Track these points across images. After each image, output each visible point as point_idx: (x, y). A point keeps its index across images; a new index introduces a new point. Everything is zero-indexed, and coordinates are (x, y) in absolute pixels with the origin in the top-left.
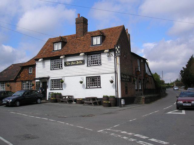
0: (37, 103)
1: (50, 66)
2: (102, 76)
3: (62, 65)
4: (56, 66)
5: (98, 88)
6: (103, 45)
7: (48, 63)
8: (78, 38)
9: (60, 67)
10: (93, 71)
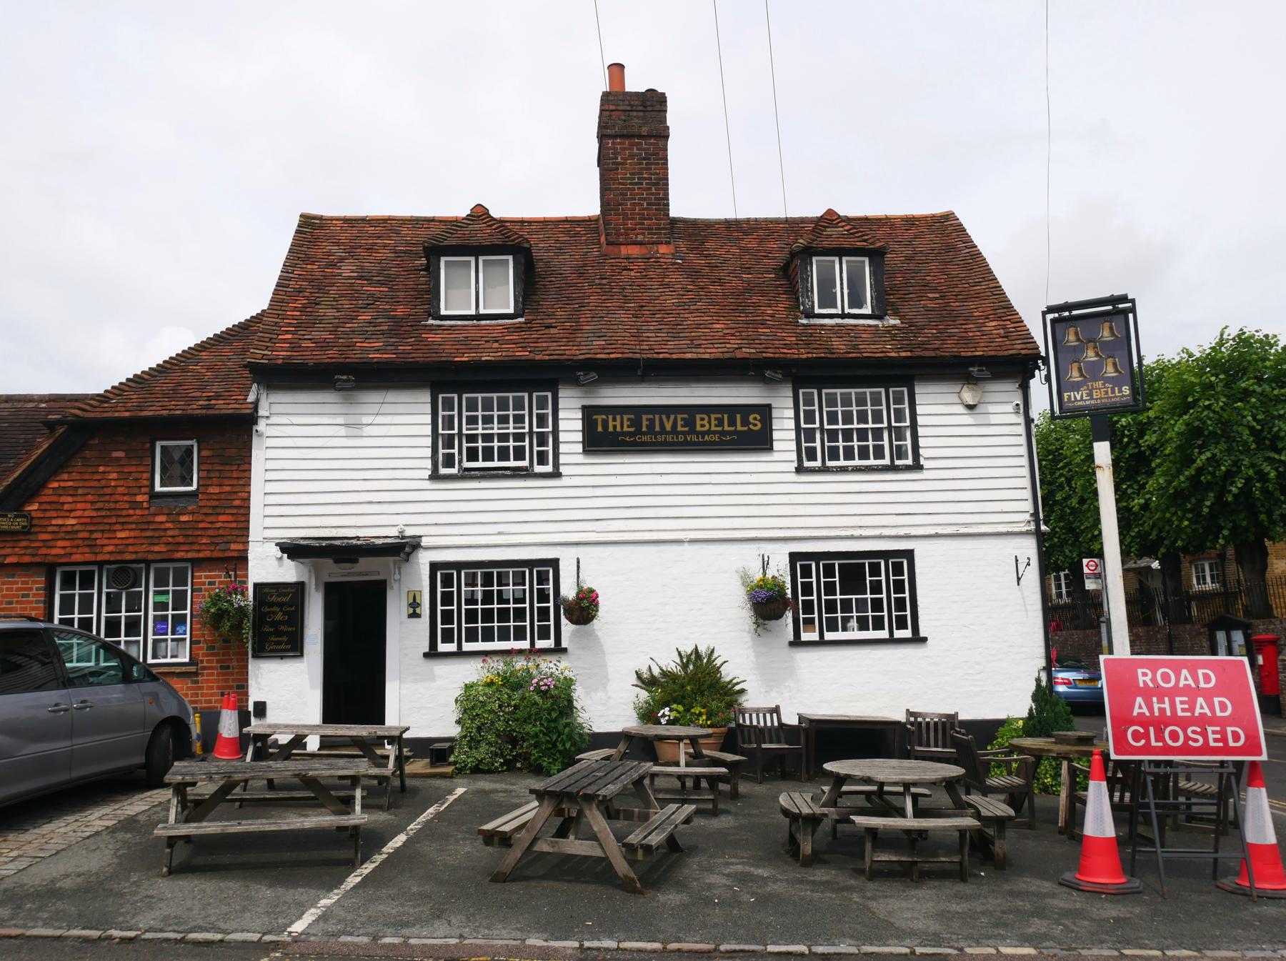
1: (429, 441)
2: (922, 551)
5: (892, 641)
7: (400, 427)
9: (531, 459)
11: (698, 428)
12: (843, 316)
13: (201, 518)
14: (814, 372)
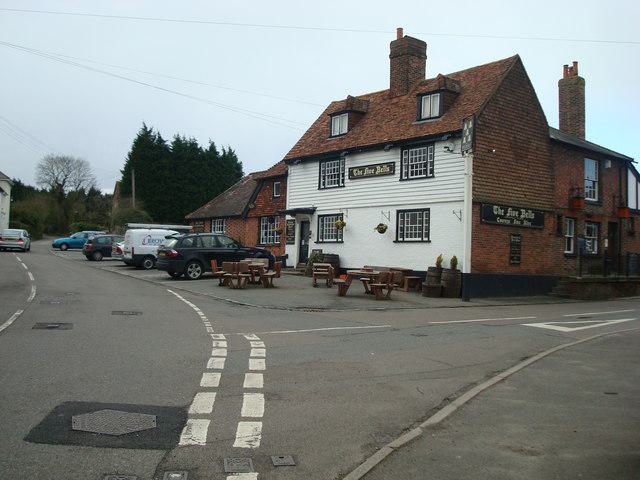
0: (188, 278)
2: (433, 208)
3: (343, 174)
4: (332, 180)
5: (422, 241)
6: (443, 120)
7: (314, 169)
8: (395, 100)
9: (338, 181)
14: (403, 145)
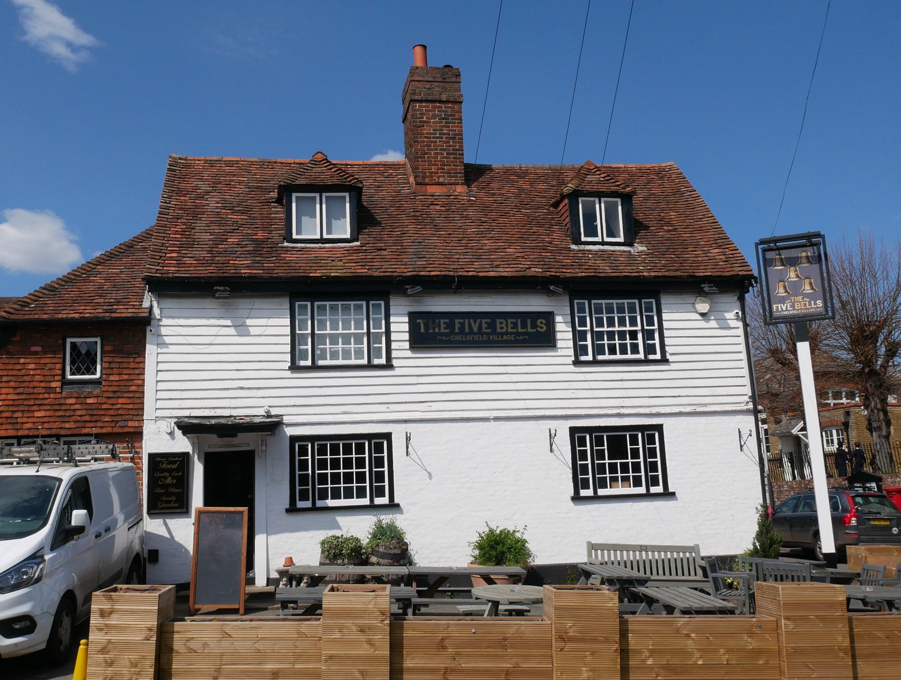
5: (648, 496)
10: (614, 394)
11: (498, 330)
12: (603, 243)
13: (101, 400)
